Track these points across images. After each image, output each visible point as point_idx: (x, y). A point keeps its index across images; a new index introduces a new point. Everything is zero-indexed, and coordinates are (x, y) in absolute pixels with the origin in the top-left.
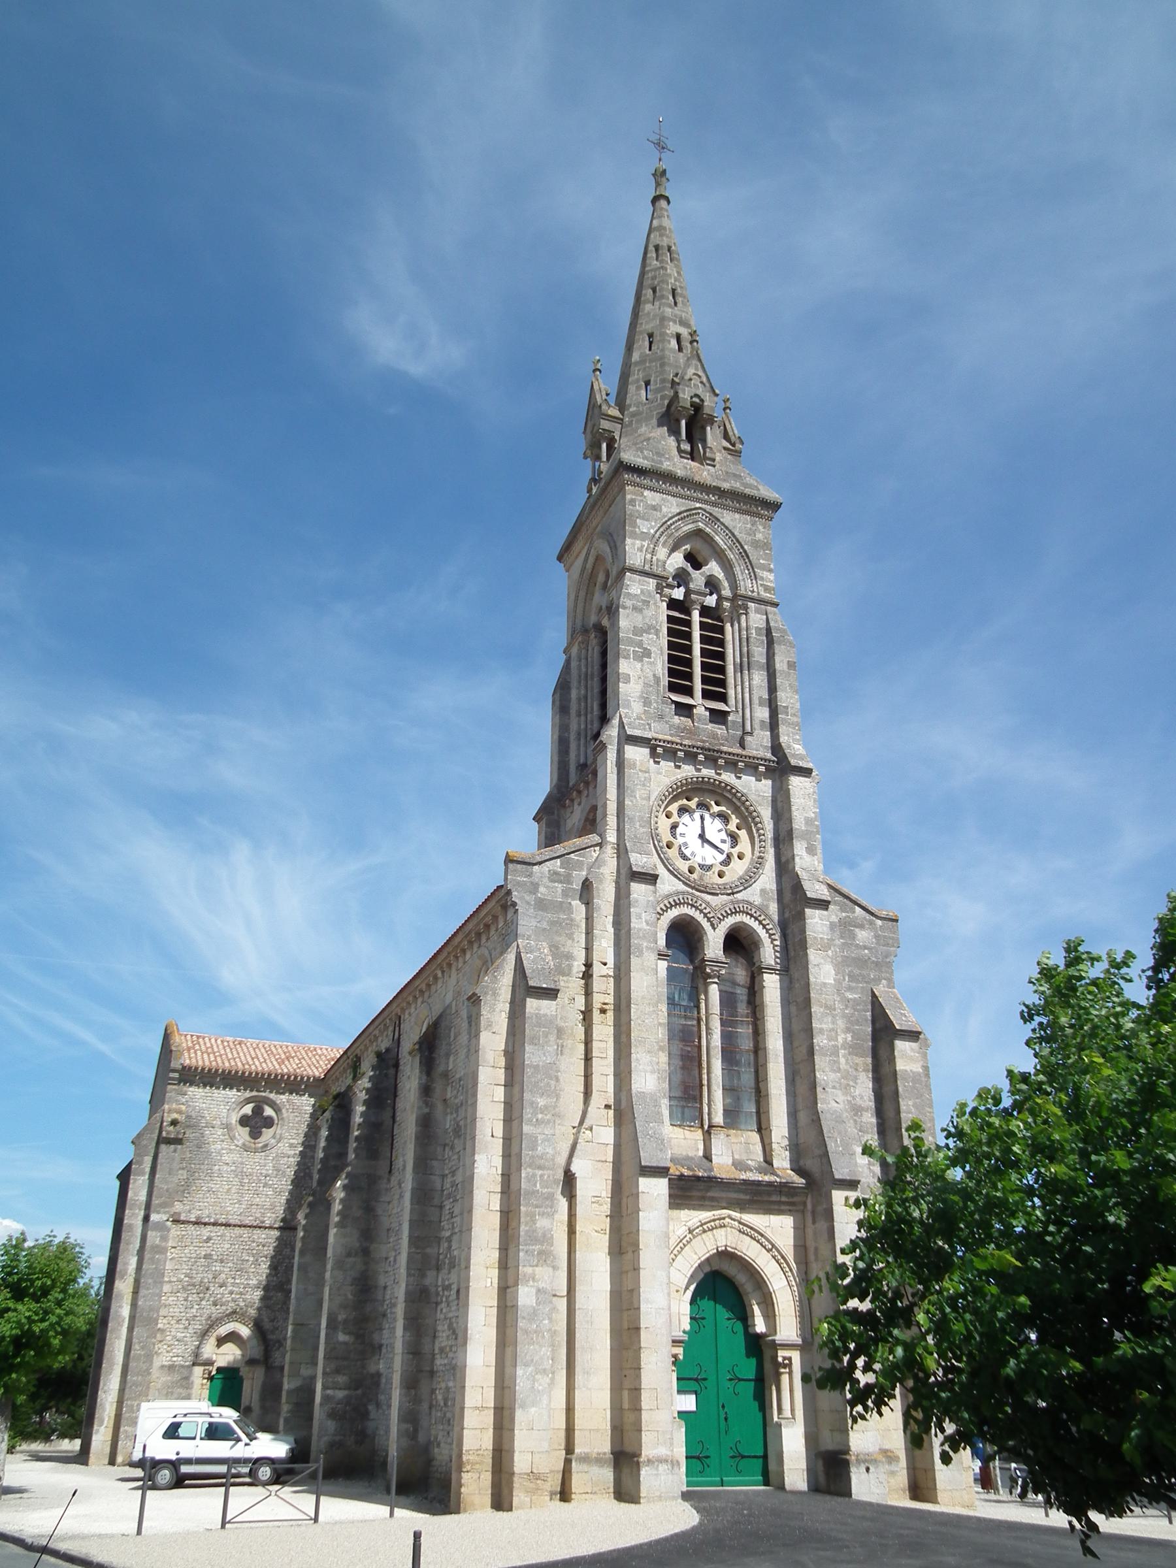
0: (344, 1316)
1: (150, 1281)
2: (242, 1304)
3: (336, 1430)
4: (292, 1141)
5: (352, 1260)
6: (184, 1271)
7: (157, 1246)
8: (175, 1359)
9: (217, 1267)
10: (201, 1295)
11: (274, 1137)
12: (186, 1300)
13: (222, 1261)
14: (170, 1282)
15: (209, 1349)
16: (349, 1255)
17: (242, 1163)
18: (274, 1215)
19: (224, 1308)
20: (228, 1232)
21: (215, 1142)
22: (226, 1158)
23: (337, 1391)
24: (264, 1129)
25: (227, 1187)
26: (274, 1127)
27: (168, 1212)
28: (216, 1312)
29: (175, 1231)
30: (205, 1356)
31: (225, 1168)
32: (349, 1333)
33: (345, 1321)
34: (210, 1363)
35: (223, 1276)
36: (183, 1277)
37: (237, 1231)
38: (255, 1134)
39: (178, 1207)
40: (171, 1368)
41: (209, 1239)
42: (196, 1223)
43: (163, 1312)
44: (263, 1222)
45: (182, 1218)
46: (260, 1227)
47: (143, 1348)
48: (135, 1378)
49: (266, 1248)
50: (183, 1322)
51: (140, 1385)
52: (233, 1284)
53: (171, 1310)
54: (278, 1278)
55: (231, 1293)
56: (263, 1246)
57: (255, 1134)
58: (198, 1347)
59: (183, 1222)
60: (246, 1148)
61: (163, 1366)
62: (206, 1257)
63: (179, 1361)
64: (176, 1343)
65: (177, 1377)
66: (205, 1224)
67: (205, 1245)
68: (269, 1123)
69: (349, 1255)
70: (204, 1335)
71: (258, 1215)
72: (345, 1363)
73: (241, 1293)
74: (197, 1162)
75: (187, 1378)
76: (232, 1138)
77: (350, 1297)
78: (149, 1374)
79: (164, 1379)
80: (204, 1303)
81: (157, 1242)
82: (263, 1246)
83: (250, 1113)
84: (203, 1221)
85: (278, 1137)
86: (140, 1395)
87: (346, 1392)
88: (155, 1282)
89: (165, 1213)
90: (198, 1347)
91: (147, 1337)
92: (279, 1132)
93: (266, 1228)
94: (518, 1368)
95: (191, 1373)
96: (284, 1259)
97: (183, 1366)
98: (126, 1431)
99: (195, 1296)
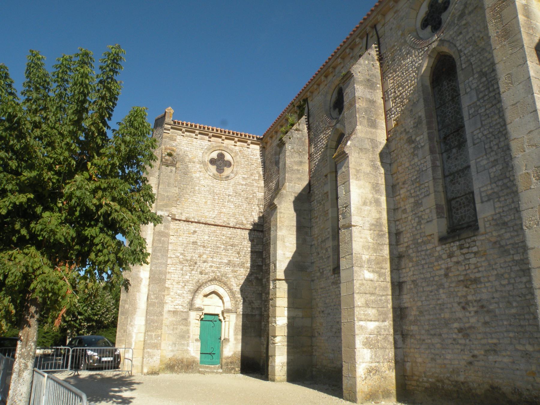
0: (367, 257)
1: (159, 254)
2: (219, 274)
3: (371, 358)
4: (244, 176)
5: (367, 208)
6: (180, 251)
7: (162, 232)
8: (177, 307)
9: (201, 250)
10: (192, 267)
11: (232, 172)
12: (182, 270)
13: (204, 247)
14: (171, 258)
15: (199, 301)
16: (365, 204)
17: (213, 186)
18: (235, 220)
19: (207, 276)
20: (207, 229)
21: (195, 172)
22: (202, 182)
23: (369, 323)
24: (225, 168)
25: (204, 200)
26: (232, 166)
27: (169, 211)
28: (204, 278)
29: (173, 225)
30: (197, 306)
31: (203, 188)
32: (373, 272)
33: (369, 261)
34: (200, 309)
35: (205, 256)
36: (179, 255)
37: (213, 228)
38: (220, 170)
39: (174, 210)
40: (175, 312)
41: (195, 232)
42: (187, 221)
43: (168, 276)
44: (229, 224)
45: (177, 218)
46: (227, 227)
47: (156, 298)
48: (152, 318)
49: (231, 241)
50: (181, 284)
51: (156, 322)
52: (213, 262)
53: (173, 276)
54: (240, 259)
55: (211, 266)
56: (230, 239)
57: (220, 170)
58: (192, 300)
59: (176, 220)
60: (215, 177)
61: (169, 311)
62: (194, 243)
63: (180, 308)
64: (177, 297)
65: (179, 318)
66: (192, 222)
67: (192, 235)
68: (229, 164)
69: (365, 204)
70: (196, 292)
71: (225, 219)
72: (373, 298)
73: (218, 268)
74: (184, 183)
75: (186, 319)
76: (207, 170)
77: (370, 240)
78: (162, 315)
79: (170, 319)
80: (193, 272)
81: (162, 230)
82: (230, 239)
83: (216, 157)
84: (190, 220)
85: (235, 172)
86: (156, 328)
87: (377, 324)
88: (162, 255)
89: (166, 211)
90: (192, 300)
91: (159, 291)
92: (235, 169)
93: (230, 227)
94: (142, 339)
95: (188, 316)
96: (243, 247)
97: (182, 312)
98: (148, 352)
99: (187, 267)
